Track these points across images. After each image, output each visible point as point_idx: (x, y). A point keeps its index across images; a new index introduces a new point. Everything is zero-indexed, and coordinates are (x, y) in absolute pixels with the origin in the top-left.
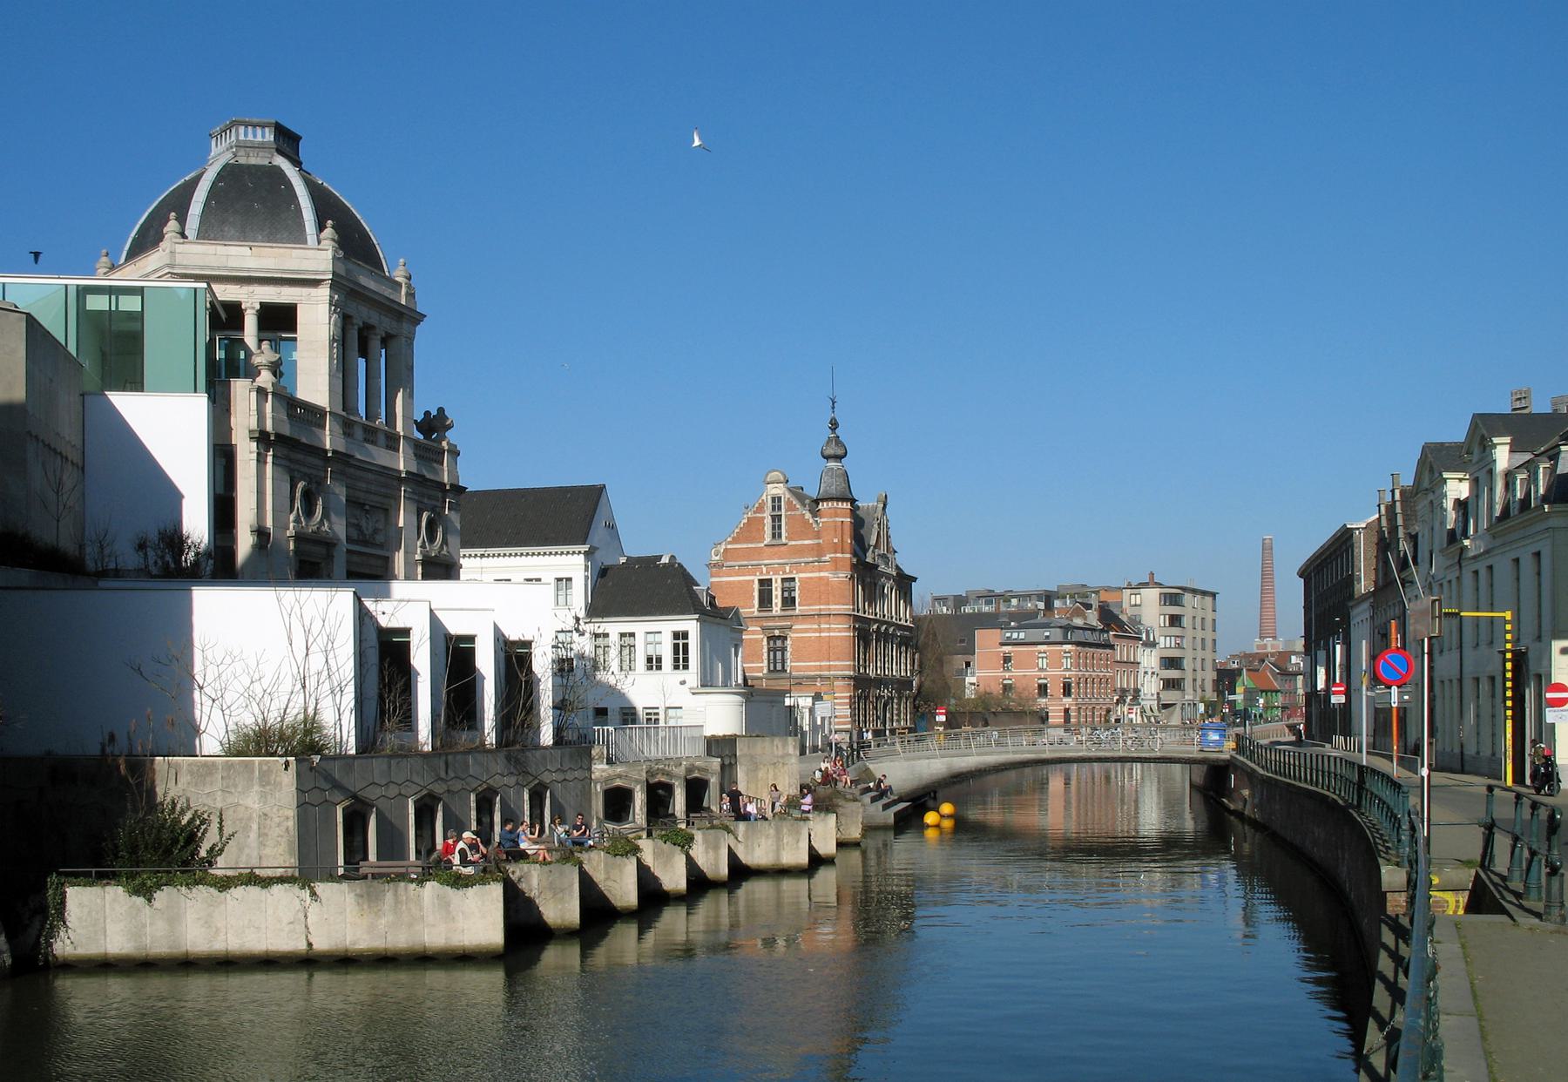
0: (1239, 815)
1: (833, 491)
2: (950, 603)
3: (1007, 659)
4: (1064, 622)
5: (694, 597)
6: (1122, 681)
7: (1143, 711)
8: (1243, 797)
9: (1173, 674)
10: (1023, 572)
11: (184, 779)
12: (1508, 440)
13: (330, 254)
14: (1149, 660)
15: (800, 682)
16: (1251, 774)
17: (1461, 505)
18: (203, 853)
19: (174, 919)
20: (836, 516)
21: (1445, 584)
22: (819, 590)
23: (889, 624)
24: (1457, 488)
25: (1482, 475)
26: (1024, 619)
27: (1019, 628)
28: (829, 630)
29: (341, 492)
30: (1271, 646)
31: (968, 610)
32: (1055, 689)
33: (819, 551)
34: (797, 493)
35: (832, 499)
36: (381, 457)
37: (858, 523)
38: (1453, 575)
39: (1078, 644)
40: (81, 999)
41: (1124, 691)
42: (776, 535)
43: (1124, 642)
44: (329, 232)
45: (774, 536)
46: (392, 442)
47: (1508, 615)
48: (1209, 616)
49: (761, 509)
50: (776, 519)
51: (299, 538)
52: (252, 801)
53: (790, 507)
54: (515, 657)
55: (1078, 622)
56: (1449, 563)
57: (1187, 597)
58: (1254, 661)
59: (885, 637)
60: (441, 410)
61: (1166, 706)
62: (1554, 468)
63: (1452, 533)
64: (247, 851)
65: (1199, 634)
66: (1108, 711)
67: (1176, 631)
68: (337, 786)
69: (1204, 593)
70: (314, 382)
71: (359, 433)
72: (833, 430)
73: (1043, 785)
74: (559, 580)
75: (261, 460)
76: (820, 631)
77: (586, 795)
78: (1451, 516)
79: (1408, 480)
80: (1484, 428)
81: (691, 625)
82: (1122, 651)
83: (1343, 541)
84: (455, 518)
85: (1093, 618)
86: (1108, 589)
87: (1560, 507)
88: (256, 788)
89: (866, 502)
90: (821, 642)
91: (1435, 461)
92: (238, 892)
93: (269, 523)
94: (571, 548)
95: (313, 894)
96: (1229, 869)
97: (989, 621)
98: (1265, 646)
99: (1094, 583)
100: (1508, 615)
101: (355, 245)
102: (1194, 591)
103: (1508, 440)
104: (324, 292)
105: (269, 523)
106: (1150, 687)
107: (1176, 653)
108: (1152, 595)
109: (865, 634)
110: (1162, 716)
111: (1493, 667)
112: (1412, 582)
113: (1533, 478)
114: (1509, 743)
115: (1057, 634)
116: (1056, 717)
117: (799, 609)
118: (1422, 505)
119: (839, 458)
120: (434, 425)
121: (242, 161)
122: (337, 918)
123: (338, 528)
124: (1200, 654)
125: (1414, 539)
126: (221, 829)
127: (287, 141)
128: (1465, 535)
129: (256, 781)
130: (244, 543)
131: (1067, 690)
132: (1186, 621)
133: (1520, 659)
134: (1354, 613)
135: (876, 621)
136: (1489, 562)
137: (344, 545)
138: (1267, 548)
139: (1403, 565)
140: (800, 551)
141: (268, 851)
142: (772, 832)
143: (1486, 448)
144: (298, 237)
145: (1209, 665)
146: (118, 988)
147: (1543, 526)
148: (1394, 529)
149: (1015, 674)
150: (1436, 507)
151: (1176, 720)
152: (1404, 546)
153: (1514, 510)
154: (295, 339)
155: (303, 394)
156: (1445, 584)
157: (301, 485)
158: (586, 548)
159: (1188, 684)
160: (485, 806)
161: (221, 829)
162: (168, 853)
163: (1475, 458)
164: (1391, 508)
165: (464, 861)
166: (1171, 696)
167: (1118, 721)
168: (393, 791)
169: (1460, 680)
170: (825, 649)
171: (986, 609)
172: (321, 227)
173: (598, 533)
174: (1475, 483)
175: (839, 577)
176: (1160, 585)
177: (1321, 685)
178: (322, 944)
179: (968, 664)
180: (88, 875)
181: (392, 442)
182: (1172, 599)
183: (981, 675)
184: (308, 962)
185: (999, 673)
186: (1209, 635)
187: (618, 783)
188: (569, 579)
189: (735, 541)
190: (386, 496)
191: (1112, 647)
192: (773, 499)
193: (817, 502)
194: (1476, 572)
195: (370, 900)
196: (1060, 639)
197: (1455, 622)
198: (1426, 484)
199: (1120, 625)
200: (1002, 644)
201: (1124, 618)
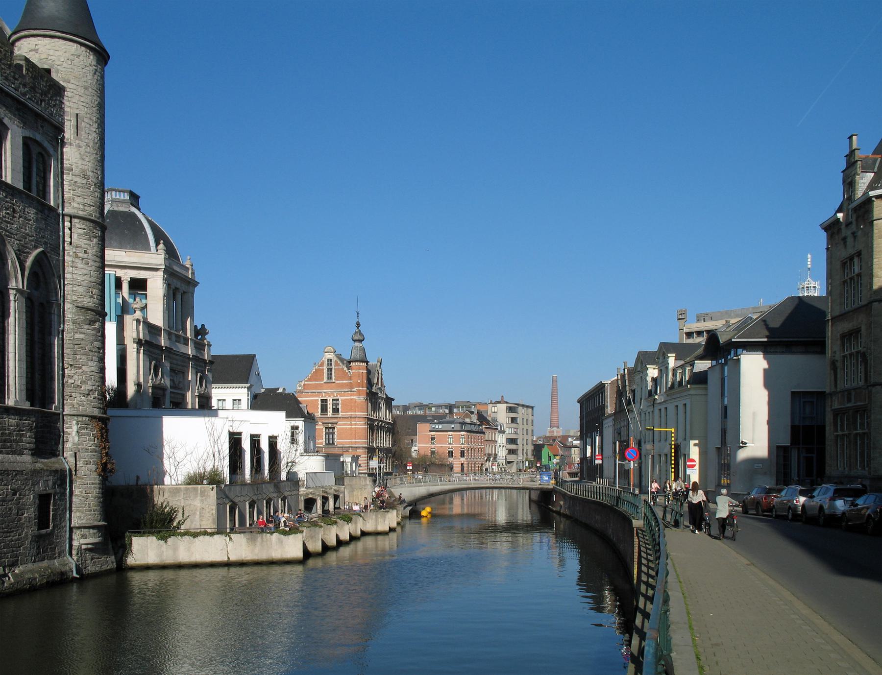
0: (558, 513)
1: (358, 357)
2: (401, 409)
3: (433, 439)
4: (462, 421)
5: (300, 409)
6: (488, 450)
7: (498, 465)
8: (561, 505)
9: (513, 447)
10: (438, 395)
11: (166, 495)
13: (163, 256)
14: (501, 439)
15: (346, 449)
16: (564, 495)
17: (654, 380)
18: (175, 524)
19: (175, 549)
20: (359, 369)
23: (382, 422)
24: (653, 372)
25: (663, 368)
26: (441, 419)
27: (439, 423)
29: (168, 365)
30: (558, 432)
31: (410, 412)
32: (457, 454)
33: (351, 386)
34: (339, 356)
36: (182, 348)
37: (369, 372)
39: (468, 431)
40: (136, 578)
41: (490, 455)
42: (329, 378)
43: (490, 431)
44: (161, 246)
46: (186, 341)
47: (673, 430)
48: (530, 418)
49: (322, 365)
50: (330, 370)
51: (154, 387)
52: (197, 503)
54: (255, 441)
55: (468, 420)
57: (520, 408)
58: (551, 441)
59: (380, 428)
60: (203, 326)
61: (509, 463)
63: (650, 391)
65: (526, 427)
67: (514, 425)
68: (227, 497)
69: (528, 407)
70: (157, 317)
71: (174, 338)
72: (358, 327)
73: (451, 499)
74: (219, 400)
75: (138, 352)
77: (297, 501)
78: (650, 384)
79: (631, 364)
80: (666, 348)
81: (300, 423)
82: (488, 435)
83: (600, 389)
84: (210, 375)
85: (474, 418)
86: (480, 404)
87: (694, 386)
89: (373, 362)
90: (351, 431)
91: (644, 359)
92: (201, 538)
93: (142, 380)
94: (241, 385)
95: (230, 538)
96: (552, 537)
97: (423, 419)
98: (553, 432)
99: (473, 401)
100: (673, 430)
101: (171, 253)
102: (523, 406)
104: (160, 274)
105: (142, 380)
106: (502, 453)
108: (503, 407)
109: (373, 426)
110: (507, 467)
111: (666, 451)
112: (632, 411)
113: (684, 373)
114: (12, 304)
115: (457, 427)
116: (457, 468)
117: (341, 414)
118: (637, 378)
119: (360, 341)
120: (200, 332)
121: (116, 209)
122: (238, 547)
123: (167, 382)
124: (526, 437)
125: (633, 391)
127: (134, 199)
128: (656, 393)
130: (131, 390)
131: (462, 454)
132: (519, 421)
133: (677, 448)
134: (605, 422)
137: (169, 390)
138: (554, 381)
139: (629, 403)
141: (203, 523)
143: (665, 358)
144: (147, 248)
146: (152, 575)
147: (686, 393)
149: (437, 446)
150: (643, 379)
151: (514, 469)
152: (629, 395)
153: (676, 386)
154: (146, 295)
155: (151, 320)
157: (153, 363)
158: (248, 385)
159: (520, 452)
160: (268, 503)
162: (163, 524)
163: (661, 361)
164: (623, 376)
165: (285, 525)
166: (511, 458)
167: (486, 470)
168: (242, 499)
170: (353, 434)
171: (419, 412)
172: (157, 244)
173: (253, 378)
174: (660, 371)
175: (359, 398)
176: (506, 402)
177: (589, 454)
178: (233, 558)
179: (412, 441)
180: (140, 532)
181: (186, 341)
182: (511, 409)
183: (420, 446)
184: (228, 564)
185: (429, 445)
186: (530, 428)
187: (310, 496)
188: (240, 400)
189: (309, 380)
190: (183, 366)
191: (484, 433)
193: (350, 362)
195: (252, 540)
196: (459, 429)
197: (651, 432)
198: (639, 369)
199: (488, 422)
201: (490, 419)
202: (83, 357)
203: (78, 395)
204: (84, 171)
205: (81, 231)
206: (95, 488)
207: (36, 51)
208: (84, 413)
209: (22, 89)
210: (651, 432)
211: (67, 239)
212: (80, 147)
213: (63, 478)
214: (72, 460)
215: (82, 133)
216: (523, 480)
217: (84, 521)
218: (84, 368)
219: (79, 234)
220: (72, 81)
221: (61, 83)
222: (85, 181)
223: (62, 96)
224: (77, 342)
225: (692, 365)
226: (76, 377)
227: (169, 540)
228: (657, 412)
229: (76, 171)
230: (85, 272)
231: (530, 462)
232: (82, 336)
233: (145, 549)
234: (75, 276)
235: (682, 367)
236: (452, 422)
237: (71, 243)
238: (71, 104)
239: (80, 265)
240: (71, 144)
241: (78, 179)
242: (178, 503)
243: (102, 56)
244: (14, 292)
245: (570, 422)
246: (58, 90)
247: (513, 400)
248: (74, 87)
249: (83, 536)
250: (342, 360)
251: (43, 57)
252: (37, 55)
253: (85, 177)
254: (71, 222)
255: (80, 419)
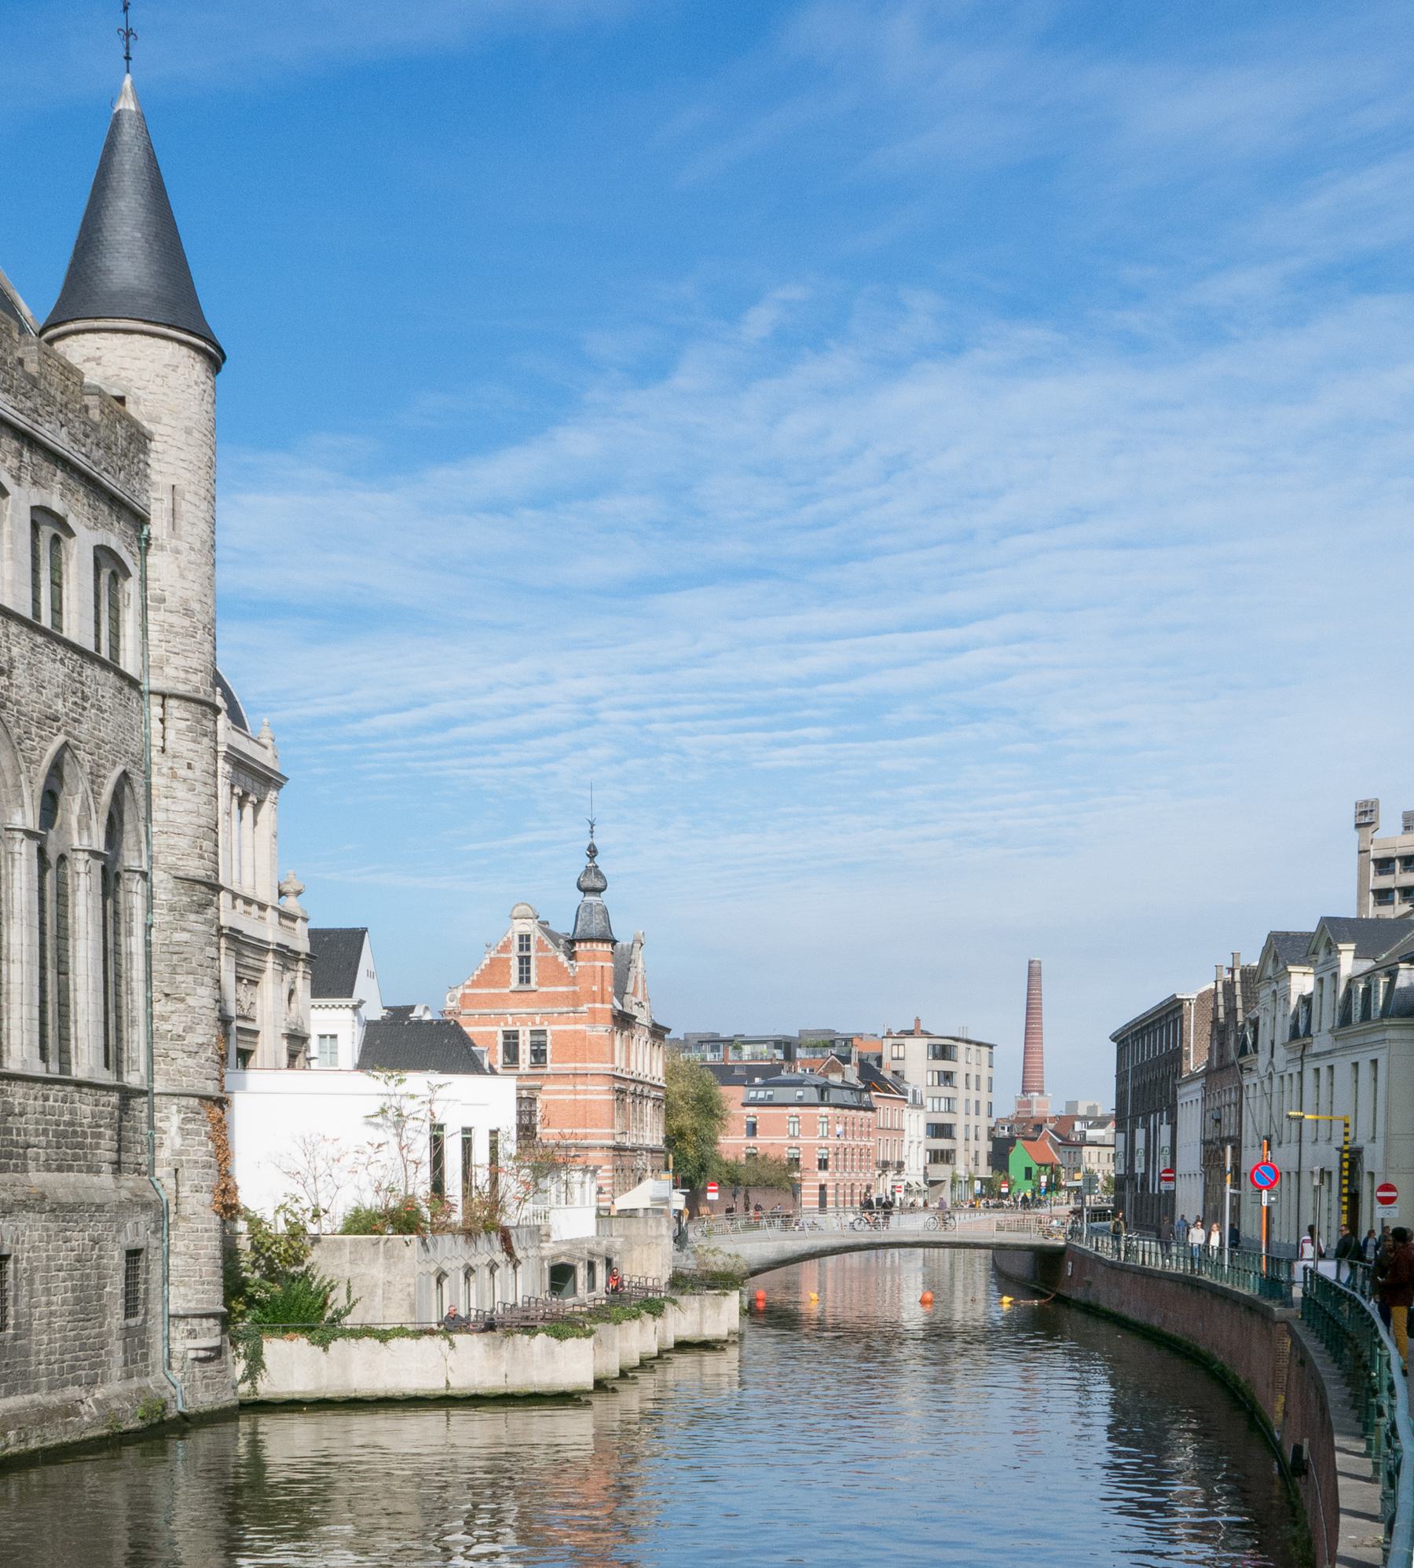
1: (595, 929)
4: (821, 1080)
9: (942, 1144)
12: (1352, 946)
14: (914, 1124)
17: (1306, 1001)
21: (1286, 1078)
22: (577, 1046)
24: (1302, 982)
25: (1327, 976)
26: (769, 1075)
28: (585, 1092)
33: (575, 1000)
35: (591, 940)
38: (1294, 1069)
42: (524, 978)
45: (521, 980)
48: (985, 1073)
49: (506, 948)
50: (524, 961)
53: (541, 947)
55: (835, 1078)
56: (1292, 1056)
57: (961, 1046)
61: (933, 1183)
62: (1391, 985)
64: (372, 1312)
65: (973, 1095)
66: (869, 1188)
67: (946, 1091)
76: (576, 1092)
80: (1333, 930)
82: (886, 1110)
83: (1170, 1012)
85: (852, 1073)
88: (381, 1260)
89: (624, 941)
91: (1284, 949)
94: (337, 1001)
95: (452, 1345)
99: (844, 1029)
102: (969, 1042)
103: (1352, 946)
107: (945, 1119)
117: (551, 1067)
119: (597, 891)
126: (349, 1292)
129: (381, 1255)
132: (959, 1079)
134: (1180, 1092)
135: (633, 1081)
136: (1330, 1062)
138: (1033, 973)
140: (553, 999)
142: (696, 1305)
143: (1331, 949)
145: (983, 1134)
147: (1379, 1037)
148: (1231, 1012)
156: (1286, 1078)
158: (351, 1002)
161: (349, 1292)
164: (1229, 987)
166: (941, 1171)
169: (1298, 1174)
176: (926, 1034)
182: (943, 1052)
186: (984, 1097)
187: (563, 1260)
188: (334, 1037)
189: (475, 984)
191: (873, 1110)
192: (521, 937)
194: (1317, 1070)
196: (816, 1100)
200: (744, 1105)
201: (888, 1075)
202: (191, 978)
203: (180, 1054)
204: (186, 601)
205: (183, 725)
206: (210, 1239)
207: (97, 360)
208: (191, 1090)
209: (98, 454)
210: (1295, 1124)
211: (157, 741)
212: (178, 552)
213: (160, 1215)
214: (170, 1183)
215: (184, 526)
216: (982, 1225)
217: (192, 1305)
218: (190, 1001)
219: (178, 731)
220: (165, 420)
221: (145, 423)
222: (186, 622)
223: (145, 450)
224: (177, 949)
225: (1392, 975)
226: (174, 1017)
227: (333, 1345)
228: (1309, 1075)
229: (172, 602)
230: (190, 806)
231: (984, 1182)
232: (185, 936)
233: (291, 1365)
234: (171, 816)
235: (1369, 975)
236: (798, 1084)
237: (163, 750)
238: (163, 467)
239: (181, 791)
240: (162, 548)
241: (174, 619)
242: (338, 1272)
243: (215, 360)
244: (86, 856)
245: (1084, 1078)
246: (140, 439)
247: (943, 1026)
248: (169, 431)
249: (192, 1334)
250: (553, 937)
251: (110, 372)
252: (99, 370)
253: (188, 613)
254: (163, 706)
255: (184, 1101)
